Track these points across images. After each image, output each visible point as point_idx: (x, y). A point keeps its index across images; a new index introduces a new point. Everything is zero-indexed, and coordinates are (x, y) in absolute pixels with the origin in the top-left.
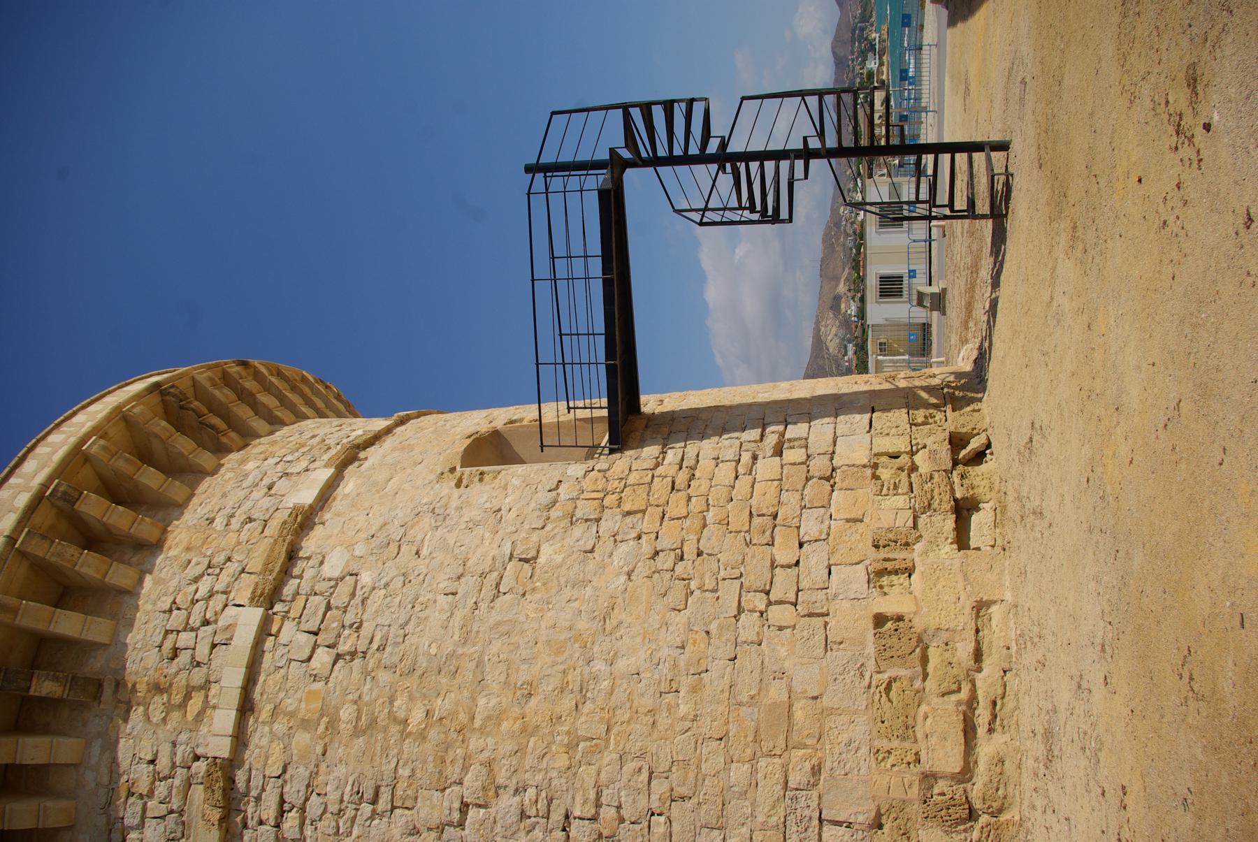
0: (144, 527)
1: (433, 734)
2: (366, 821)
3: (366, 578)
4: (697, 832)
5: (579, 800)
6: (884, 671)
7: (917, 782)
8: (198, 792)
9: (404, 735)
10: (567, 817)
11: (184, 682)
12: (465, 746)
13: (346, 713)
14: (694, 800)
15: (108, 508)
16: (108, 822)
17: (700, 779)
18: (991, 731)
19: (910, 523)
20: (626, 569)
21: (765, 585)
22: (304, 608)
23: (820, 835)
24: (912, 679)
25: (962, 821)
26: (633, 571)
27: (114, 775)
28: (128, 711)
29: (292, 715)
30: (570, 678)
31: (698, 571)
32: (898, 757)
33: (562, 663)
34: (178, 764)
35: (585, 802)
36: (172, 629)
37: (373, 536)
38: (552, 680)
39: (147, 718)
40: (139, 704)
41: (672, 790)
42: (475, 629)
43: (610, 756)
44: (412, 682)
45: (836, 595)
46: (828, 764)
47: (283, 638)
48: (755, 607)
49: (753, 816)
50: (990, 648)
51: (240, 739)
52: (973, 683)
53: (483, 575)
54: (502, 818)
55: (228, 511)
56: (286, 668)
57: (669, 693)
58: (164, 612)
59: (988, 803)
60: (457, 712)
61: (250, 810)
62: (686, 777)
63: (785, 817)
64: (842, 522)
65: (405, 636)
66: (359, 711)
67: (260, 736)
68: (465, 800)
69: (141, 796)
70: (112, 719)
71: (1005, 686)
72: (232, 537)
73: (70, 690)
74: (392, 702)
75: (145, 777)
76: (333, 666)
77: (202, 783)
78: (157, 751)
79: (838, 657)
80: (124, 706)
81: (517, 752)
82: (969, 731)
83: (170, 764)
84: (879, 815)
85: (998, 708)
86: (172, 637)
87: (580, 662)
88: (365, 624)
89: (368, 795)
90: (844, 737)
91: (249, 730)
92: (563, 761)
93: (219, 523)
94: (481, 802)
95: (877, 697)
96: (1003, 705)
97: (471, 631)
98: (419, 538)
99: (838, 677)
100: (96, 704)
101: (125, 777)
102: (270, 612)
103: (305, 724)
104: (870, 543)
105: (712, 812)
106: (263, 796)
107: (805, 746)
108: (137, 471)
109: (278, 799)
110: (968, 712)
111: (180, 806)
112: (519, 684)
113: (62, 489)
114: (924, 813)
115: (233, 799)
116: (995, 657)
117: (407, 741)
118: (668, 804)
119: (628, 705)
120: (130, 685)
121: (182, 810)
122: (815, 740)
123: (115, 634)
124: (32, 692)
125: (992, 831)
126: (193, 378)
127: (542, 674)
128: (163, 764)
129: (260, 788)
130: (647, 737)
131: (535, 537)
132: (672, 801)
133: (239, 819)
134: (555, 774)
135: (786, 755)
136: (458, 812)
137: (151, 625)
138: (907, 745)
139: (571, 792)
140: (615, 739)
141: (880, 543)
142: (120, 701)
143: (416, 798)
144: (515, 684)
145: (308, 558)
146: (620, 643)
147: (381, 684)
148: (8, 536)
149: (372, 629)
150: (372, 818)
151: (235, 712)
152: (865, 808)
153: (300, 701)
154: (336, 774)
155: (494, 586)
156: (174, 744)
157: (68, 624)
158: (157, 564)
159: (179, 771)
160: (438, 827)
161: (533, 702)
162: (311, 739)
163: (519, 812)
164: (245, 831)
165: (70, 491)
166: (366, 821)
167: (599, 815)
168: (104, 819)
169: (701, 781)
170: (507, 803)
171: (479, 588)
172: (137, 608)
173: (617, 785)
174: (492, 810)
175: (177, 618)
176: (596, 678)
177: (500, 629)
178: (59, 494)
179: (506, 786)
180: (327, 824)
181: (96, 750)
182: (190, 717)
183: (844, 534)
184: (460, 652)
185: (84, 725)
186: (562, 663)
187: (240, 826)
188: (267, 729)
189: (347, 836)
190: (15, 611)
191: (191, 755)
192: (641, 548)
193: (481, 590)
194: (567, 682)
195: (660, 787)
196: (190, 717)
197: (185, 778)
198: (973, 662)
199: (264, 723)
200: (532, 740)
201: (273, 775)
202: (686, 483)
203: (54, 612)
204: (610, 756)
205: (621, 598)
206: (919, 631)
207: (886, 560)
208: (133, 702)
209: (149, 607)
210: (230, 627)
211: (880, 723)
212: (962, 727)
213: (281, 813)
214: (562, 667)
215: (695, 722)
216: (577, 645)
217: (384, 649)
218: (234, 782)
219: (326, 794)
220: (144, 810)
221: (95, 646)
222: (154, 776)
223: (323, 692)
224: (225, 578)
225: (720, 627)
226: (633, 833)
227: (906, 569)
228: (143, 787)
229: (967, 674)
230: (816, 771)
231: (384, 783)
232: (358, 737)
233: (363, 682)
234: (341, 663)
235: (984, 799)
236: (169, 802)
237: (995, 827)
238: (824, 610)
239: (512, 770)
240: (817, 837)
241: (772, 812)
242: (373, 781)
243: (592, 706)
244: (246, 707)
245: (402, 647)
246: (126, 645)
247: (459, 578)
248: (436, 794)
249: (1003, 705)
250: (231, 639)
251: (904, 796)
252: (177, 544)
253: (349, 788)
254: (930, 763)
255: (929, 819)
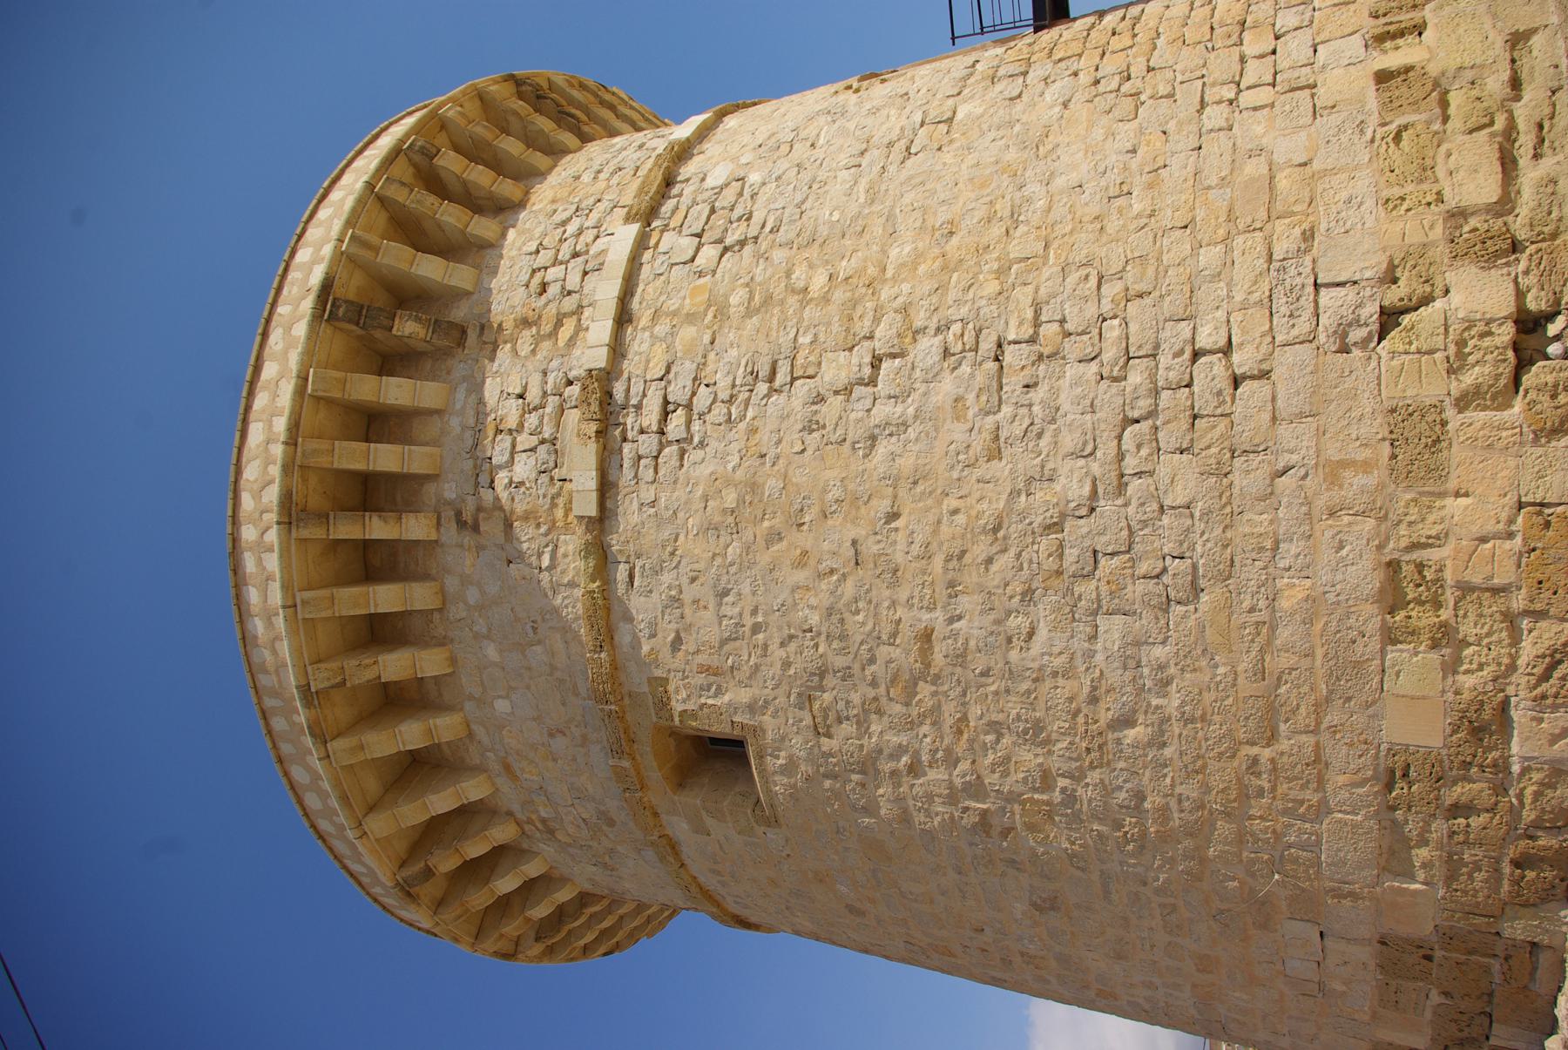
0: (507, 188)
1: (839, 295)
2: (762, 399)
3: (754, 178)
4: (1160, 327)
5: (1013, 323)
6: (1391, 122)
7: (1441, 221)
8: (573, 416)
9: (804, 304)
10: (1000, 346)
11: (554, 311)
12: (875, 298)
13: (737, 298)
14: (1156, 294)
15: (468, 166)
16: (475, 467)
17: (1161, 272)
18: (1537, 156)
20: (1061, 100)
21: (1233, 77)
22: (686, 217)
23: (1316, 302)
24: (1429, 123)
25: (1505, 253)
26: (1070, 101)
27: (481, 416)
28: (494, 351)
29: (674, 314)
30: (998, 207)
32: (1414, 200)
33: (988, 195)
34: (549, 392)
35: (1021, 324)
36: (540, 266)
37: (760, 146)
38: (976, 213)
39: (515, 352)
40: (506, 342)
41: (1127, 289)
42: (883, 188)
43: (1051, 270)
44: (814, 252)
45: (1324, 67)
46: (1323, 226)
47: (662, 248)
48: (1222, 97)
49: (1230, 297)
50: (1531, 73)
51: (617, 349)
52: (1510, 113)
53: (890, 145)
54: (921, 361)
55: (596, 167)
56: (666, 274)
57: (1119, 196)
58: (531, 254)
59: (1538, 229)
60: (865, 268)
61: (629, 421)
62: (1143, 274)
63: (1271, 290)
64: (1329, 11)
65: (802, 213)
66: (751, 293)
67: (639, 342)
68: (877, 352)
69: (510, 431)
70: (477, 361)
71: (1554, 105)
72: (601, 185)
73: (433, 333)
74: (788, 275)
75: (514, 411)
76: (720, 259)
77: (576, 407)
78: (527, 383)
79: (1329, 121)
80: (490, 347)
81: (937, 289)
82: (1508, 164)
83: (541, 394)
84: (1392, 267)
85: (1546, 130)
86: (539, 275)
87: (1010, 189)
88: (755, 214)
89: (764, 372)
90: (1344, 195)
91: (627, 340)
92: (992, 287)
93: (586, 178)
94: (896, 350)
95: (1382, 150)
96: (1552, 126)
97: (879, 192)
98: (814, 133)
99: (1331, 138)
100: (460, 350)
101: (493, 416)
102: (648, 229)
103: (691, 318)
105: (1177, 303)
106: (645, 402)
107: (1293, 214)
109: (661, 400)
110: (1505, 143)
111: (552, 434)
112: (937, 226)
113: (419, 143)
114: (1451, 252)
115: (611, 413)
116: (1539, 80)
117: (807, 309)
118: (1123, 304)
119: (1070, 217)
120: (495, 326)
121: (555, 438)
122: (1306, 204)
123: (478, 282)
124: (394, 331)
125: (1545, 257)
126: (549, 79)
127: (964, 211)
128: (533, 395)
129: (641, 394)
130: (1093, 243)
131: (951, 102)
132: (1128, 301)
133: (617, 432)
134: (984, 302)
135: (1269, 227)
136: (870, 367)
137: (517, 268)
138: (1425, 186)
139: (1003, 317)
140: (1055, 253)
141: (1380, 13)
142: (485, 343)
143: (820, 363)
144: (933, 227)
145: (687, 180)
146: (1056, 164)
147: (776, 262)
149: (764, 215)
150: (768, 396)
151: (611, 322)
152: (1373, 262)
153: (685, 298)
154: (726, 360)
156: (545, 373)
157: (430, 269)
159: (550, 399)
160: (846, 388)
161: (955, 240)
162: (698, 331)
163: (942, 350)
164: (624, 444)
165: (428, 146)
166: (762, 399)
167: (1038, 335)
168: (471, 462)
169: (1162, 274)
170: (927, 349)
172: (501, 256)
173: (1059, 299)
174: (910, 358)
175: (544, 258)
176: (1029, 200)
177: (912, 182)
178: (416, 148)
179: (926, 328)
180: (719, 412)
181: (461, 394)
182: (561, 343)
184: (866, 211)
185: (448, 373)
186: (988, 195)
187: (619, 439)
188: (647, 334)
189: (741, 421)
190: (376, 250)
191: (564, 380)
195: (1111, 290)
196: (561, 343)
197: (558, 404)
198: (1509, 90)
199: (644, 329)
200: (955, 275)
201: (655, 377)
203: (415, 256)
204: (1051, 270)
205: (1056, 126)
206: (1434, 75)
207: (1386, 24)
208: (500, 341)
209: (514, 253)
210: (603, 252)
211: (1388, 174)
212: (1497, 155)
213: (665, 414)
214: (989, 198)
215: (1153, 218)
216: (1005, 176)
217: (778, 231)
218: (611, 396)
219: (715, 383)
220: (514, 446)
221: (459, 295)
222: (523, 409)
223: (709, 284)
224: (594, 216)
225: (1180, 124)
226: (1081, 344)
227: (1415, 27)
228: (512, 422)
229: (1502, 104)
230: (1309, 236)
231: (782, 356)
232: (752, 317)
233: (755, 264)
234: (729, 254)
235: (1531, 225)
236: (540, 433)
237: (1549, 251)
238: (1311, 81)
239: (932, 308)
240: (1312, 304)
241: (1254, 288)
242: (770, 357)
243: (1026, 229)
244: (623, 317)
245: (799, 223)
246: (490, 290)
247: (862, 154)
248: (843, 354)
249: (1552, 126)
250: (602, 264)
251: (1425, 240)
252: (541, 200)
253: (742, 369)
254: (1457, 199)
255: (1458, 258)
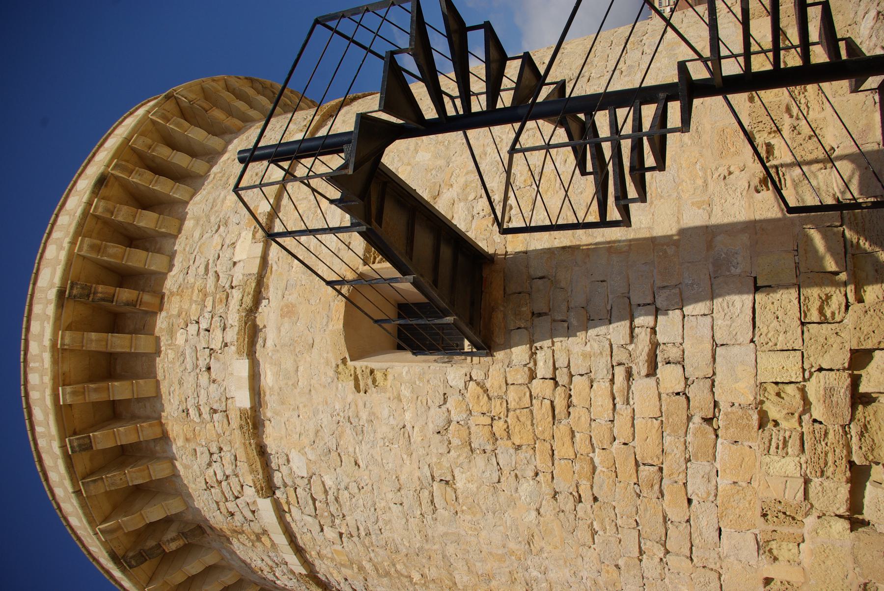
19: (800, 494)
31: (598, 516)
104: (758, 512)
108: (109, 392)
113: (75, 444)
123: (186, 503)
148: (74, 492)
155: (430, 503)
157: (154, 513)
158: (175, 453)
171: (418, 503)
178: (77, 449)
183: (732, 500)
192: (541, 488)
193: (421, 503)
194: (515, 579)
202: (570, 441)
